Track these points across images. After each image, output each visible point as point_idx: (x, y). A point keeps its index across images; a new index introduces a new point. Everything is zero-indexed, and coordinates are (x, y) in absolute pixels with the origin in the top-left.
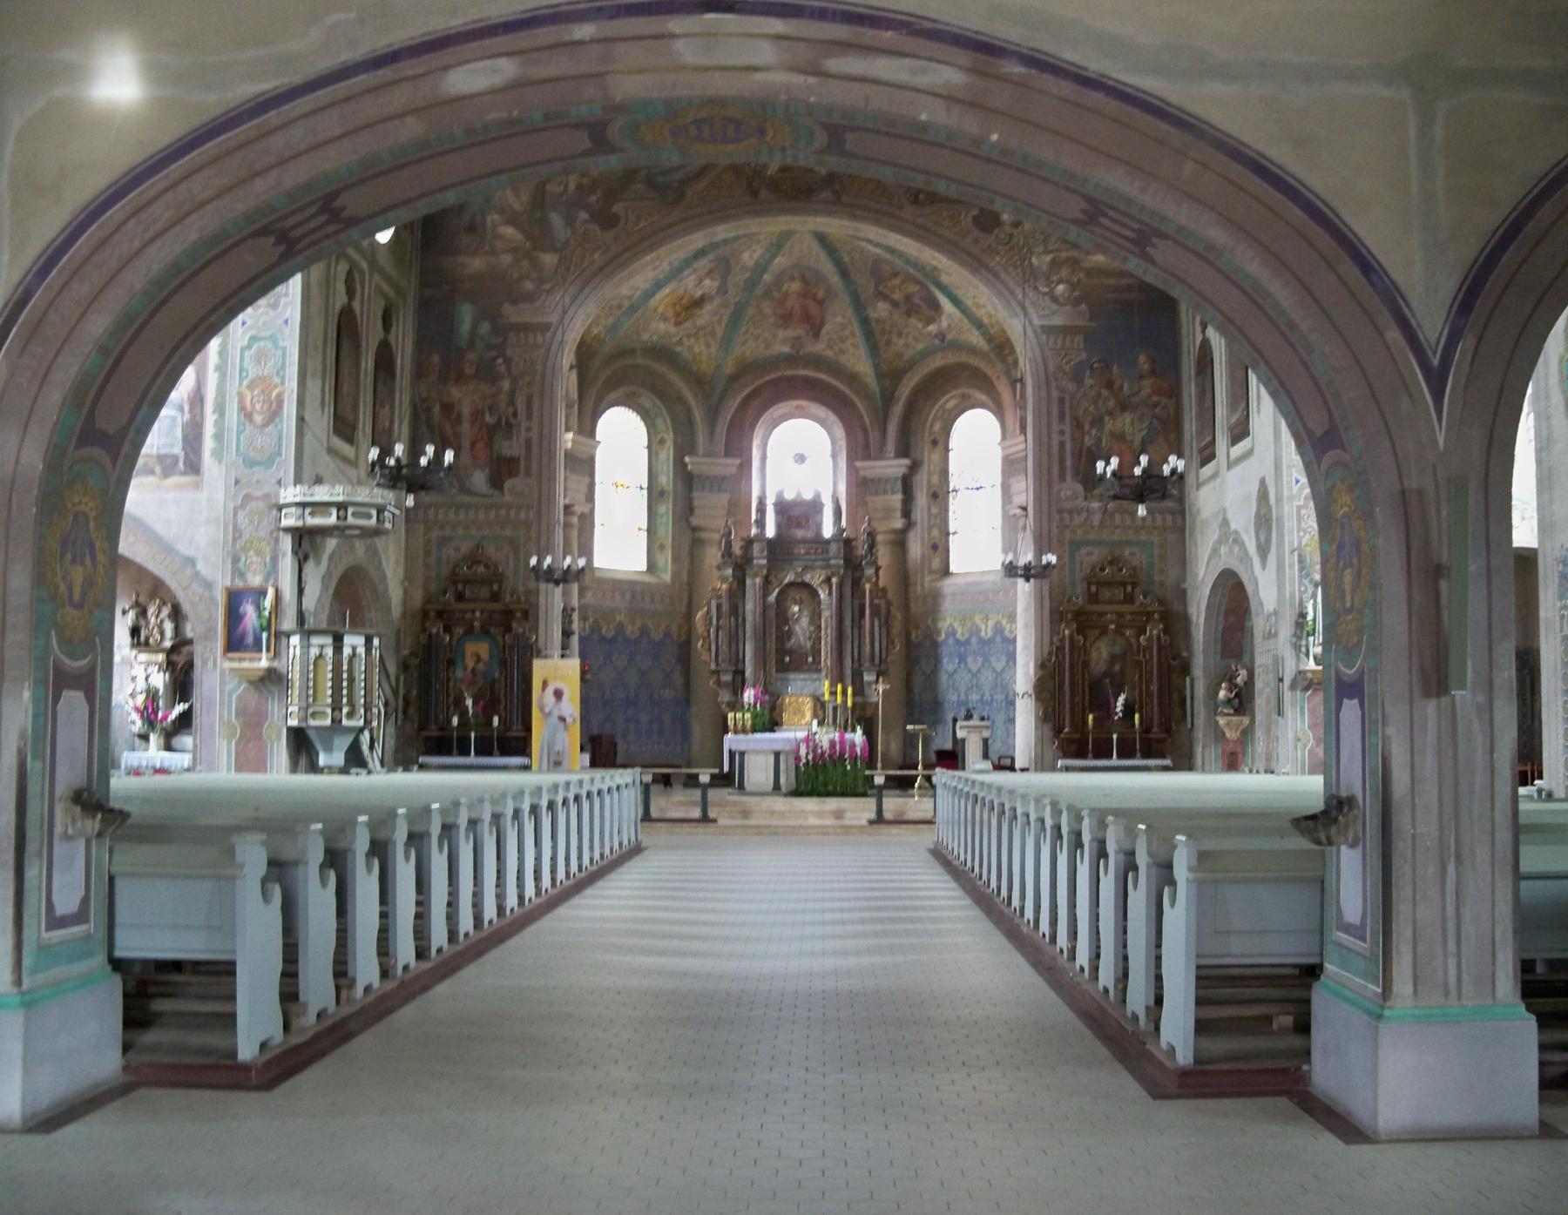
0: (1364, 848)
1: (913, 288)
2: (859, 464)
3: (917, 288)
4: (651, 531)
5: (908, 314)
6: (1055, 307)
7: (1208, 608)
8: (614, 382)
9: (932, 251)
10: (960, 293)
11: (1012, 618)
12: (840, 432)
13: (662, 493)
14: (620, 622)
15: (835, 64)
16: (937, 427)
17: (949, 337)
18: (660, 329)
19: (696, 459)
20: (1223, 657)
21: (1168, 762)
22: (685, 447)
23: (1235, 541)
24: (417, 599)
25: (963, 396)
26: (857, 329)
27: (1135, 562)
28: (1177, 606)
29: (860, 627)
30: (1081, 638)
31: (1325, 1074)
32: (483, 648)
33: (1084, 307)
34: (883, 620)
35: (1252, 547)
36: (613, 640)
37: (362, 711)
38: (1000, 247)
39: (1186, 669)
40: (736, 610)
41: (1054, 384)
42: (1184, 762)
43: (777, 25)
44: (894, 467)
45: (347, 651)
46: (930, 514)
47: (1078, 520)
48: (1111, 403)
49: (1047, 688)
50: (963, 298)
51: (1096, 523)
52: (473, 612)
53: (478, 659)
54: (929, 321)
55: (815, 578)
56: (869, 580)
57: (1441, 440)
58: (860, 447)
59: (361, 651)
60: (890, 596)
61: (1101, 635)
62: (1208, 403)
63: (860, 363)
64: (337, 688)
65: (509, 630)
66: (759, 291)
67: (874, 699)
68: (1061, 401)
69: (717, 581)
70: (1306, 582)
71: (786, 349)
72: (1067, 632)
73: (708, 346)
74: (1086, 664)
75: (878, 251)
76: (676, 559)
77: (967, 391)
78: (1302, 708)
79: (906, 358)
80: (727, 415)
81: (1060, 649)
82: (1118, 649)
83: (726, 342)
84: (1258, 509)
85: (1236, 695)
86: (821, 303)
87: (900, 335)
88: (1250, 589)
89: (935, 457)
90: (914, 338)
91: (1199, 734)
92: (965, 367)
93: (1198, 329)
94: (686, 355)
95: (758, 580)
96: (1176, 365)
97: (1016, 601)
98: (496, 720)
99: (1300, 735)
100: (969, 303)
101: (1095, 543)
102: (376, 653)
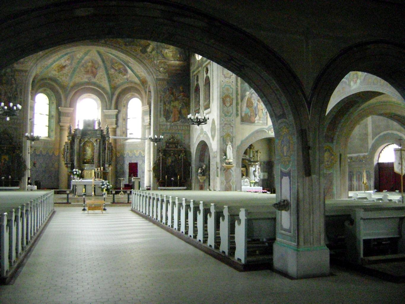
0: (290, 211)
1: (121, 66)
2: (104, 111)
3: (122, 66)
4: (49, 127)
5: (119, 73)
6: (160, 73)
7: (196, 150)
8: (40, 87)
9: (129, 58)
11: (144, 151)
12: (99, 102)
13: (52, 116)
14: (41, 150)
15: (175, 18)
17: (130, 79)
18: (53, 73)
19: (62, 108)
20: (199, 162)
21: (185, 188)
22: (59, 105)
23: (205, 134)
25: (132, 95)
26: (105, 76)
28: (188, 149)
29: (105, 153)
31: (277, 264)
32: (7, 157)
33: (167, 74)
34: (110, 151)
35: (210, 136)
36: (39, 155)
38: (147, 58)
39: (190, 164)
40: (72, 148)
42: (189, 188)
43: (162, 7)
44: (114, 112)
46: (122, 124)
47: (164, 127)
48: (173, 98)
49: (156, 170)
50: (134, 70)
52: (4, 147)
54: (125, 75)
56: (107, 141)
57: (310, 119)
58: (105, 106)
60: (112, 145)
61: (169, 156)
62: (198, 100)
63: (106, 84)
66: (81, 64)
70: (224, 144)
71: (87, 80)
72: (161, 155)
73: (66, 78)
74: (165, 163)
75: (113, 56)
76: (56, 133)
77: (134, 93)
79: (118, 84)
80: (70, 97)
81: (159, 160)
82: (173, 159)
83: (71, 77)
86: (96, 69)
87: (117, 78)
88: (209, 145)
89: (124, 110)
90: (120, 79)
95: (78, 140)
98: (10, 177)
101: (168, 133)
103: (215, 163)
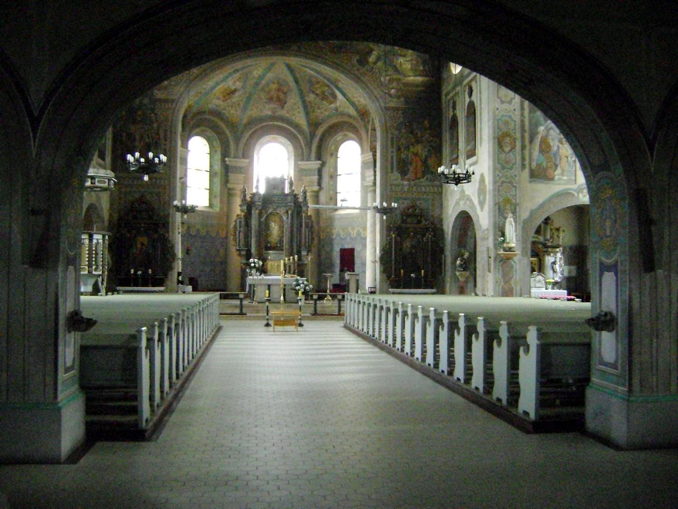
0: (617, 333)
2: (299, 163)
4: (211, 190)
5: (323, 99)
10: (346, 91)
11: (365, 229)
13: (216, 174)
16: (333, 148)
17: (339, 110)
20: (459, 246)
21: (434, 290)
22: (225, 154)
23: (468, 199)
24: (116, 216)
27: (422, 206)
28: (438, 226)
30: (399, 238)
32: (145, 240)
35: (476, 202)
36: (195, 236)
37: (101, 268)
39: (442, 251)
40: (248, 224)
41: (389, 131)
42: (441, 291)
45: (95, 241)
48: (413, 140)
49: (386, 259)
51: (406, 190)
53: (143, 244)
54: (331, 103)
55: (281, 211)
56: (304, 212)
58: (301, 155)
59: (101, 241)
63: (301, 120)
64: (90, 257)
65: (157, 232)
66: (260, 87)
67: (306, 262)
68: (392, 138)
69: (237, 210)
71: (270, 113)
72: (393, 236)
73: (236, 110)
75: (312, 72)
76: (221, 202)
78: (499, 269)
80: (244, 140)
83: (245, 109)
84: (480, 186)
85: (464, 263)
86: (285, 94)
87: (319, 108)
88: (474, 219)
90: (324, 110)
91: (448, 279)
92: (345, 123)
93: (451, 110)
94: (227, 114)
95: (257, 211)
96: (440, 125)
97: (366, 222)
99: (498, 280)
100: (350, 95)
102: (107, 242)
103: (486, 249)
